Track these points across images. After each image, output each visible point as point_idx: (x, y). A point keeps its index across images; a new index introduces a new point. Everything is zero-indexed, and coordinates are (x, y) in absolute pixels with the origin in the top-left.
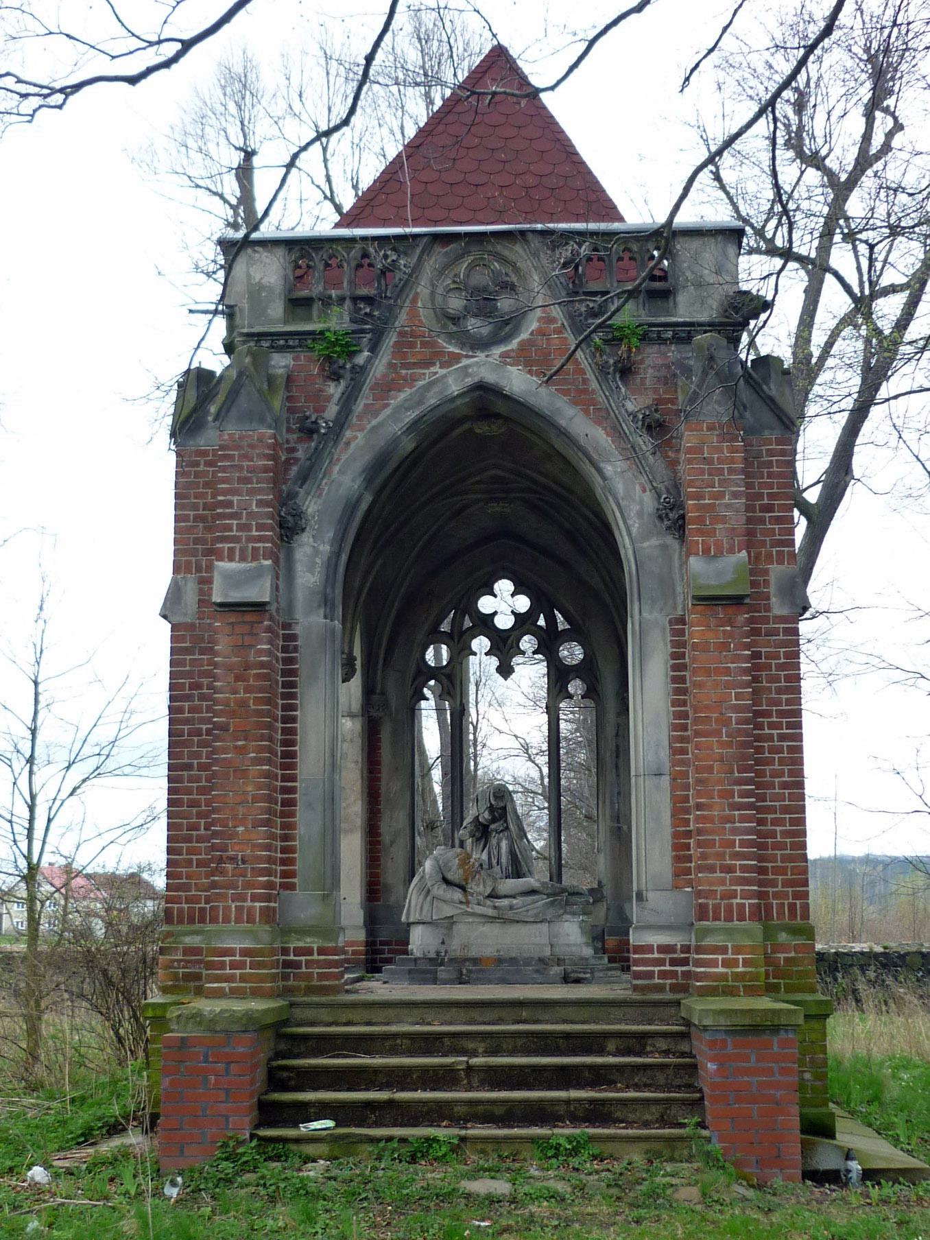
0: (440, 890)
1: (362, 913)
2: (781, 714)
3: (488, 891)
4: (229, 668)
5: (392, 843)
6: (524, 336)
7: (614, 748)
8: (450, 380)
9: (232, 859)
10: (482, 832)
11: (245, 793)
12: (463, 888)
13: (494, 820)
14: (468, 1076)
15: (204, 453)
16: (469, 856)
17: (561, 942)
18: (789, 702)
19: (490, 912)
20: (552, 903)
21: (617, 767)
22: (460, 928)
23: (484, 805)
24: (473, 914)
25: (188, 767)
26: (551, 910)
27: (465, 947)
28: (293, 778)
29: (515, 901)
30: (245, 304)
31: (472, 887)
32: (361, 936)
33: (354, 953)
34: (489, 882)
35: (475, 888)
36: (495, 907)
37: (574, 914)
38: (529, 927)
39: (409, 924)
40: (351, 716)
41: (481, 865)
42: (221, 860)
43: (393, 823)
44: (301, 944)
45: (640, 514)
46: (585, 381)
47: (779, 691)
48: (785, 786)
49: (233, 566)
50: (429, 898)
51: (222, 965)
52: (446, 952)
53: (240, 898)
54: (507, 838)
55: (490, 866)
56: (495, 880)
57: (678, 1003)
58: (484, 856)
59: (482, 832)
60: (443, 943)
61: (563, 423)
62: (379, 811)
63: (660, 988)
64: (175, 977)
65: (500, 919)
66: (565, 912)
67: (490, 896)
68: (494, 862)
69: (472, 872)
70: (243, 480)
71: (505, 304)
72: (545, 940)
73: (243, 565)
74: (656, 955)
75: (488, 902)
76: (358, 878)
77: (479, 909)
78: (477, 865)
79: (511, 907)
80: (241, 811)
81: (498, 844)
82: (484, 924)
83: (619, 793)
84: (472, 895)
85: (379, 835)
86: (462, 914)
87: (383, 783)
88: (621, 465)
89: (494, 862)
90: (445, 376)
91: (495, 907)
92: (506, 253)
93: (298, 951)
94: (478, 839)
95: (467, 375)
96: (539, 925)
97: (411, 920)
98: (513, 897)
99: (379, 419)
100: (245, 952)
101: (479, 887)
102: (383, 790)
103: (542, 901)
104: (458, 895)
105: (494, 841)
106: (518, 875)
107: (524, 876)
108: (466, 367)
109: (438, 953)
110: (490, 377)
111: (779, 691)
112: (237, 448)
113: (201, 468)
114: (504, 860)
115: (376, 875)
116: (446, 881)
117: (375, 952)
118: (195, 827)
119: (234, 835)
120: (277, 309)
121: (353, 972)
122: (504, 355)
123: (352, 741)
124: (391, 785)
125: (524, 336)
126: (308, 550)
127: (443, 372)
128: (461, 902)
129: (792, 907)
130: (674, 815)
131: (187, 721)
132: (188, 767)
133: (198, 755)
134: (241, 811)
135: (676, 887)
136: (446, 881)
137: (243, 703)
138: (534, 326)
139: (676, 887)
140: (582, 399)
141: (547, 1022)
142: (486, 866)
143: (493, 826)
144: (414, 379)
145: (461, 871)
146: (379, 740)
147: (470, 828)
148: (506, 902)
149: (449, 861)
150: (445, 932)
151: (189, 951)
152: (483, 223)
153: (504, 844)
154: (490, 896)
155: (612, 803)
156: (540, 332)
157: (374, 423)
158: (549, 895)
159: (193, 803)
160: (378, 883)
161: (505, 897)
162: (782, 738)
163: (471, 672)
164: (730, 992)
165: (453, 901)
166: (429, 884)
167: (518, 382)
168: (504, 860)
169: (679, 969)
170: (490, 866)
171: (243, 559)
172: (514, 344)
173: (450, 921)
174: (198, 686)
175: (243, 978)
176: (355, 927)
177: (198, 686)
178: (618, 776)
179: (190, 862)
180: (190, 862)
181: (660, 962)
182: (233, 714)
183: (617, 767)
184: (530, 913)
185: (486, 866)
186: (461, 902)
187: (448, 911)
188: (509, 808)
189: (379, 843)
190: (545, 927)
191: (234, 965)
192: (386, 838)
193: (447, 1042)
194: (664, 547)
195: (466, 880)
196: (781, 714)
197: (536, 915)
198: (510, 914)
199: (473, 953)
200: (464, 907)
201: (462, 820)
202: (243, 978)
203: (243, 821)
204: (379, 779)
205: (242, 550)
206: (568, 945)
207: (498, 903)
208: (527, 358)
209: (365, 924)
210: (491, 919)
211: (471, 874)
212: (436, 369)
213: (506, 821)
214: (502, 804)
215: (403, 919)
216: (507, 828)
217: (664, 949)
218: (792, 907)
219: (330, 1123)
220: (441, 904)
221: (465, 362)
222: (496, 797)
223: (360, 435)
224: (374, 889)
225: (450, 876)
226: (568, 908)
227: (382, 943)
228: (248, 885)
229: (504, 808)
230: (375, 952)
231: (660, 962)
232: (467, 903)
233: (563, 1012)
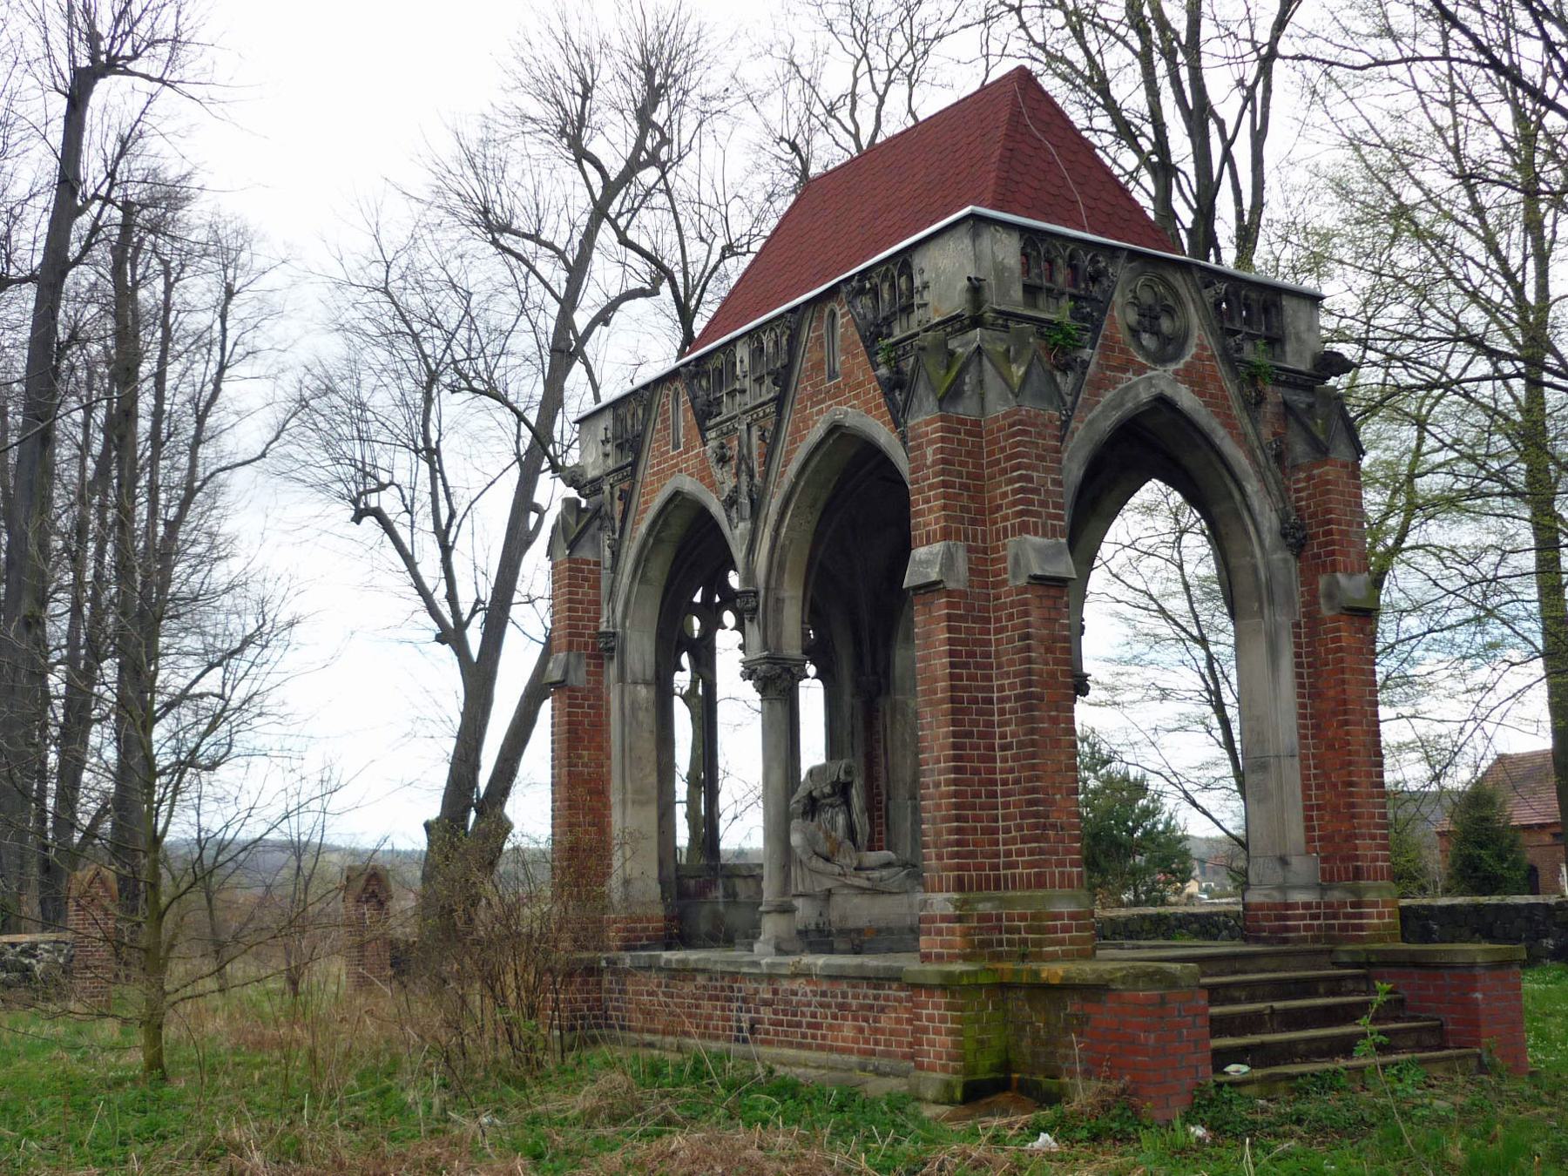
3: (855, 864)
4: (1041, 640)
6: (1188, 358)
8: (1141, 388)
9: (1053, 826)
11: (1060, 762)
14: (1271, 1020)
15: (963, 422)
19: (865, 884)
22: (837, 900)
25: (969, 734)
27: (843, 918)
30: (992, 280)
40: (646, 683)
42: (1045, 827)
45: (1270, 528)
46: (1229, 408)
49: (1038, 540)
51: (1054, 930)
53: (1061, 864)
57: (1331, 951)
61: (1218, 442)
63: (1304, 940)
64: (971, 944)
65: (874, 891)
70: (1040, 458)
71: (1166, 325)
73: (1045, 541)
80: (1058, 779)
88: (1255, 483)
90: (1136, 383)
92: (1171, 279)
95: (1152, 386)
99: (1095, 412)
100: (1072, 916)
108: (1150, 378)
109: (817, 925)
110: (1168, 392)
112: (1034, 425)
113: (962, 436)
118: (977, 795)
119: (1054, 803)
120: (1017, 293)
122: (1176, 373)
125: (1188, 358)
127: (1135, 379)
130: (1303, 791)
131: (965, 689)
132: (969, 734)
133: (976, 723)
134: (1058, 779)
135: (1308, 853)
137: (1053, 674)
138: (1194, 350)
139: (1308, 853)
140: (1229, 423)
141: (1253, 972)
144: (1115, 382)
151: (984, 918)
152: (932, 223)
156: (1197, 357)
157: (1090, 416)
159: (976, 771)
164: (1381, 939)
167: (1186, 398)
171: (1045, 535)
172: (1181, 365)
174: (972, 654)
175: (1072, 941)
177: (972, 654)
179: (975, 829)
180: (975, 829)
181: (1303, 917)
182: (1045, 685)
187: (828, 883)
191: (1066, 929)
193: (1222, 992)
194: (1285, 561)
198: (881, 887)
199: (850, 924)
203: (1060, 790)
205: (1044, 525)
208: (1191, 377)
210: (862, 890)
212: (1129, 375)
217: (1307, 906)
219: (1245, 1069)
221: (1150, 373)
223: (1081, 427)
228: (1068, 851)
231: (1303, 917)
233: (1263, 962)
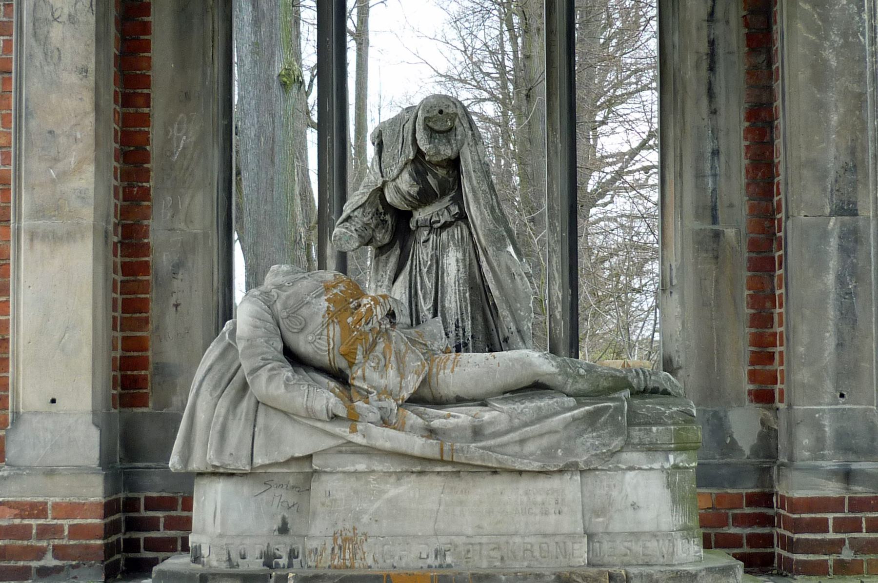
0: (276, 384)
1: (95, 435)
3: (412, 384)
5: (178, 266)
7: (704, 48)
10: (395, 229)
12: (341, 377)
13: (425, 197)
16: (358, 292)
17: (616, 526)
19: (418, 445)
20: (592, 419)
21: (711, 94)
22: (331, 488)
23: (399, 156)
24: (369, 451)
26: (589, 438)
27: (347, 541)
29: (487, 415)
31: (366, 374)
32: (94, 491)
33: (75, 531)
34: (414, 362)
35: (375, 377)
36: (431, 432)
37: (651, 449)
38: (525, 484)
39: (189, 478)
41: (391, 315)
43: (178, 220)
50: (246, 405)
52: (293, 554)
54: (460, 244)
55: (416, 319)
56: (429, 355)
58: (400, 291)
59: (395, 229)
60: (284, 529)
62: (145, 194)
65: (446, 463)
66: (628, 445)
67: (416, 400)
68: (425, 307)
69: (366, 335)
72: (571, 522)
74: (831, 535)
75: (412, 418)
76: (87, 352)
77: (384, 438)
78: (379, 312)
79: (477, 432)
81: (437, 260)
82: (399, 475)
83: (716, 153)
84: (365, 396)
85: (145, 249)
86: (339, 451)
87: (156, 132)
89: (425, 307)
91: (431, 432)
94: (381, 250)
96: (555, 483)
97: (195, 465)
98: (482, 401)
101: (384, 376)
102: (154, 148)
103: (561, 414)
104: (325, 397)
105: (423, 253)
106: (491, 340)
107: (505, 344)
109: (269, 559)
114: (452, 302)
115: (141, 345)
116: (294, 358)
117: (134, 525)
123: (72, 19)
124: (175, 133)
128: (334, 418)
136: (294, 358)
142: (403, 318)
143: (421, 215)
145: (335, 331)
146: (146, 28)
147: (360, 219)
148: (460, 417)
149: (303, 303)
150: (290, 498)
153: (453, 263)
154: (416, 400)
155: (699, 175)
158: (580, 396)
160: (142, 363)
161: (459, 401)
163: (369, 118)
165: (311, 415)
166: (246, 367)
168: (452, 302)
170: (416, 319)
173: (305, 470)
176: (80, 470)
178: (714, 112)
183: (711, 94)
184: (531, 447)
185: (403, 318)
186: (334, 418)
187: (298, 441)
188: (468, 163)
189: (145, 268)
190: (570, 487)
192: (162, 258)
195: (349, 356)
197: (548, 453)
198: (474, 451)
200: (341, 430)
201: (343, 199)
204: (145, 120)
206: (635, 535)
207: (440, 418)
209: (106, 461)
210: (420, 465)
211: (363, 340)
213: (458, 199)
214: (447, 152)
215: (174, 462)
216: (462, 217)
220: (277, 422)
222: (432, 132)
225: (304, 345)
226: (637, 433)
227: (152, 504)
229: (454, 164)
230: (134, 525)
232: (353, 419)
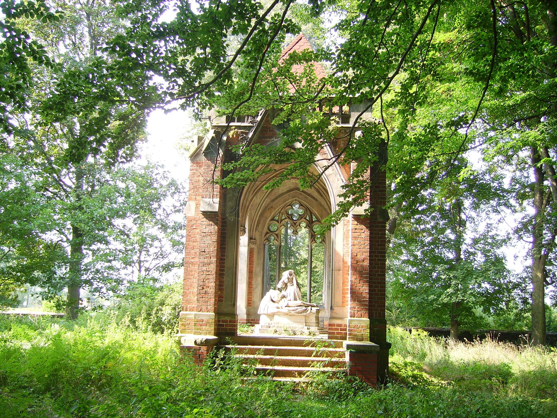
2: (379, 252)
5: (256, 287)
18: (382, 249)
28: (224, 267)
44: (224, 319)
47: (378, 245)
48: (379, 275)
93: (223, 321)
102: (254, 271)
111: (378, 245)
121: (244, 311)
126: (231, 195)
129: (380, 314)
162: (379, 260)
169: (343, 332)
196: (379, 252)
202: (338, 329)
218: (380, 314)
224: (249, 303)
225: (274, 299)
227: (251, 320)
